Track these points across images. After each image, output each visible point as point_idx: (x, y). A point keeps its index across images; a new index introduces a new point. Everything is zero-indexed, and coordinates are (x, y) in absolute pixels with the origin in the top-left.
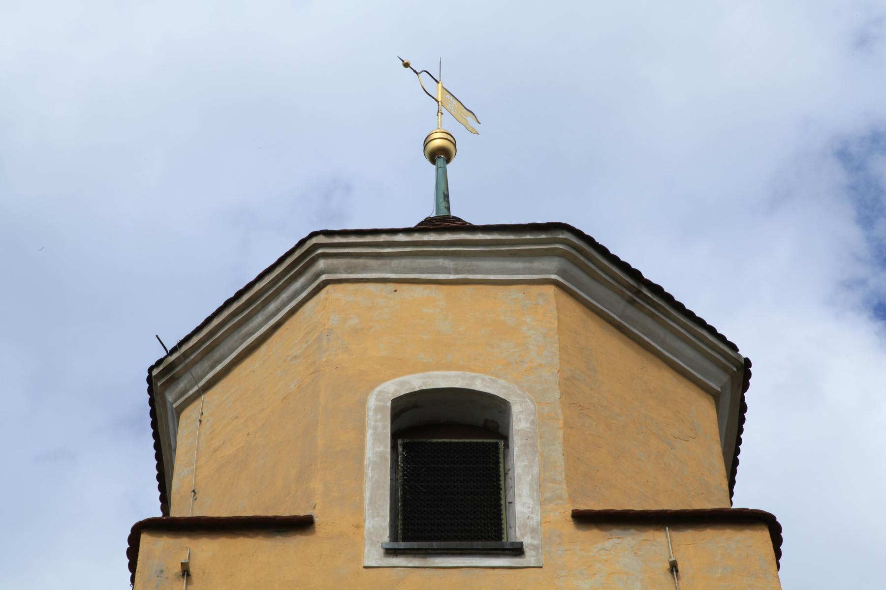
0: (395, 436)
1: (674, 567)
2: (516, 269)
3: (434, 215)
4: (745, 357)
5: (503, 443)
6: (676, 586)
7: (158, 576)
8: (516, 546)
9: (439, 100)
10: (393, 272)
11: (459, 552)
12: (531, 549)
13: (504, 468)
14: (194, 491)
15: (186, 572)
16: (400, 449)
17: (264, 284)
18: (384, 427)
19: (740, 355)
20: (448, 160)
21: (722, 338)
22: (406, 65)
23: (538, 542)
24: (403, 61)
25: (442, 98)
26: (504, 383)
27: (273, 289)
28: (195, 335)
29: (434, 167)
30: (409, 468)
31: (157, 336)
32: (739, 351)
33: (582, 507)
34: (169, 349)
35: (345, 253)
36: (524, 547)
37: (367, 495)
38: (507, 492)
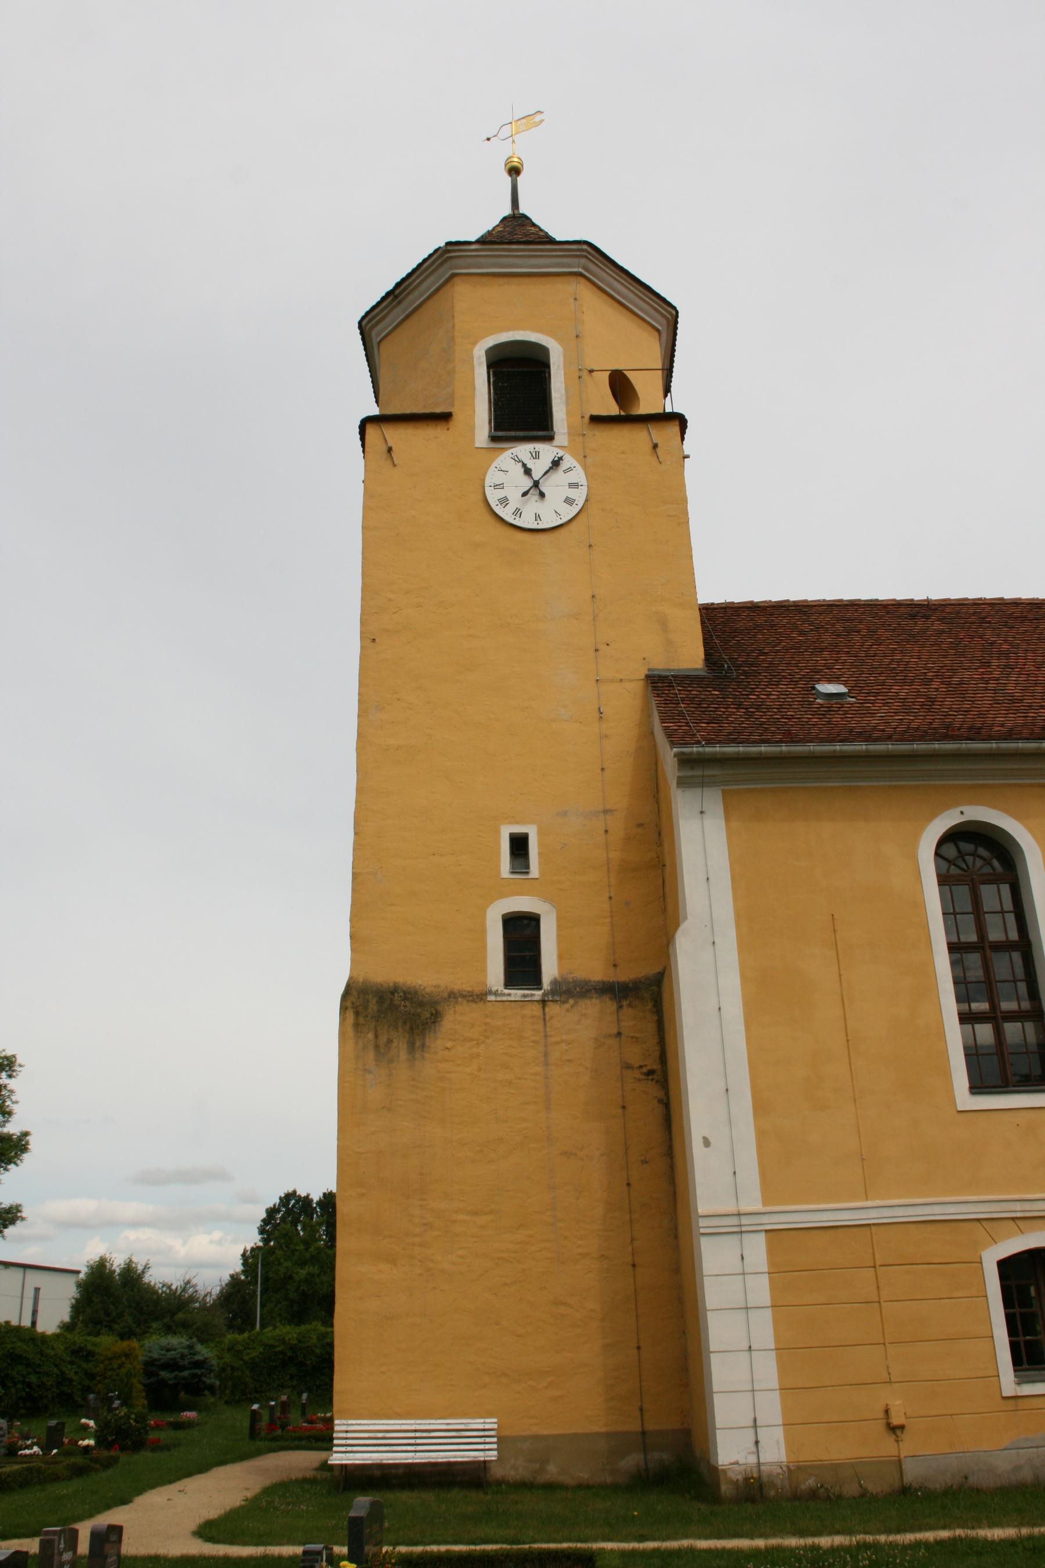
21: (430, 256)
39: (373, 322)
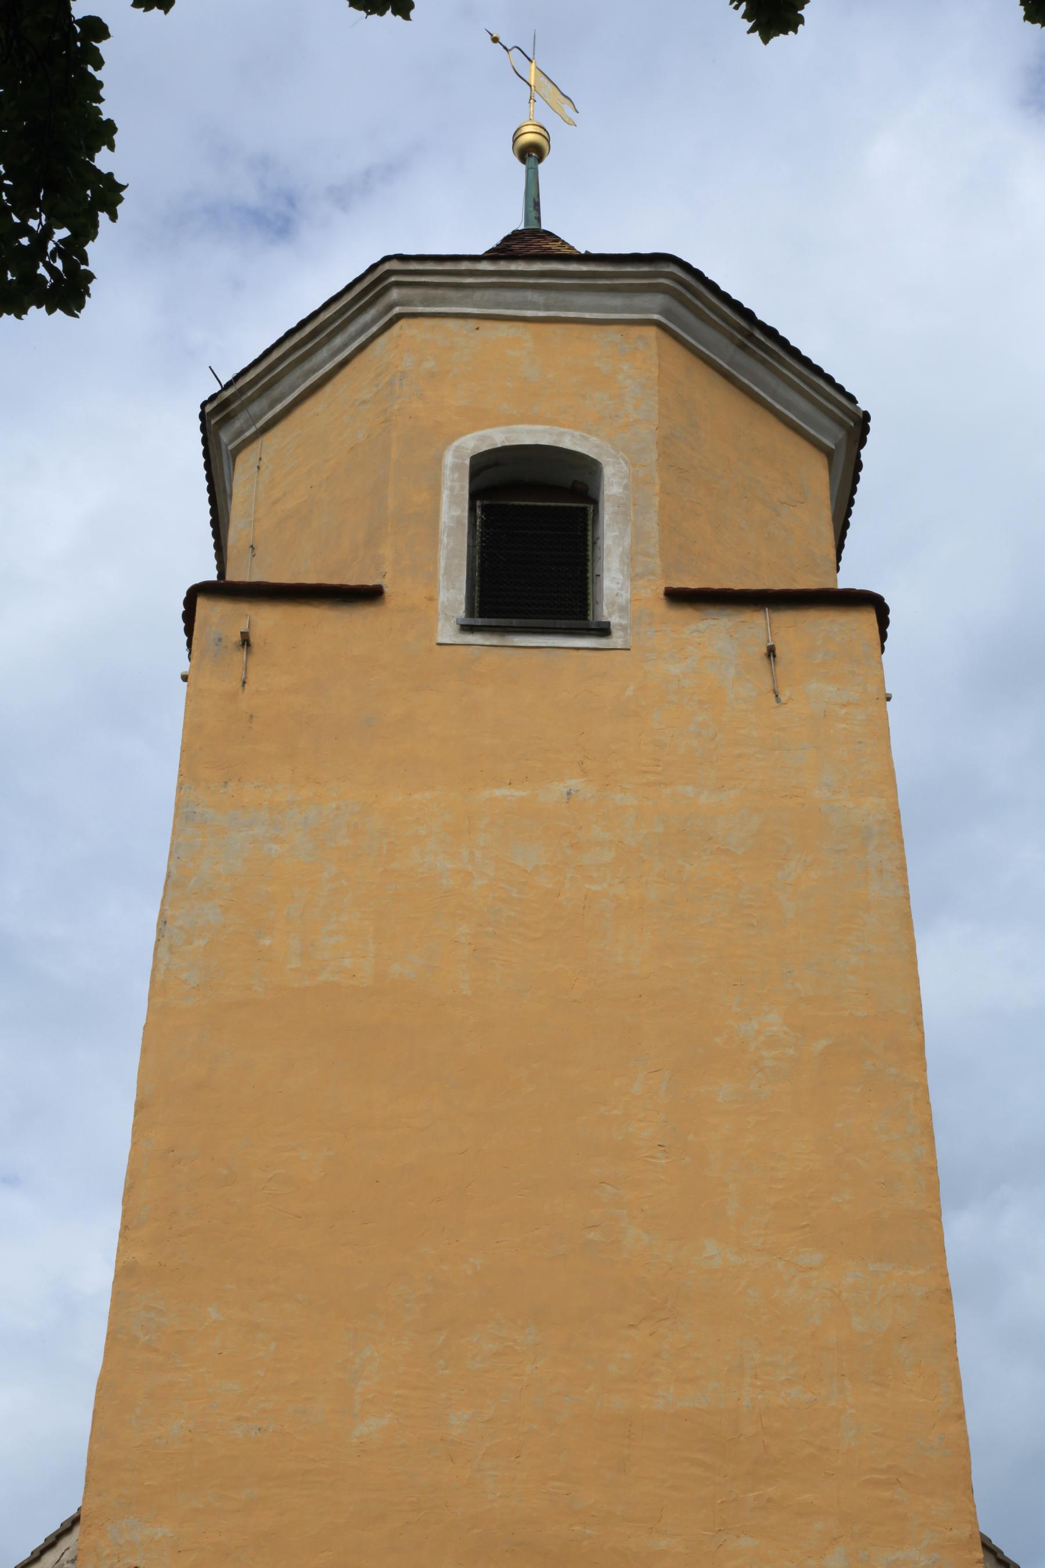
0: (473, 496)
1: (771, 652)
2: (613, 306)
3: (522, 227)
4: (864, 410)
5: (592, 509)
6: (772, 673)
7: (216, 645)
8: (602, 626)
9: (532, 83)
10: (475, 306)
11: (541, 630)
12: (618, 629)
13: (593, 536)
14: (252, 546)
15: (246, 641)
16: (479, 512)
17: (330, 315)
18: (462, 488)
19: (859, 408)
20: (540, 159)
21: (840, 389)
22: (495, 40)
23: (626, 622)
24: (491, 35)
25: (535, 81)
26: (594, 440)
27: (340, 321)
28: (253, 369)
29: (523, 167)
30: (488, 534)
31: (210, 367)
32: (857, 402)
33: (677, 584)
34: (223, 384)
35: (422, 282)
36: (611, 627)
37: (442, 563)
38: (595, 564)
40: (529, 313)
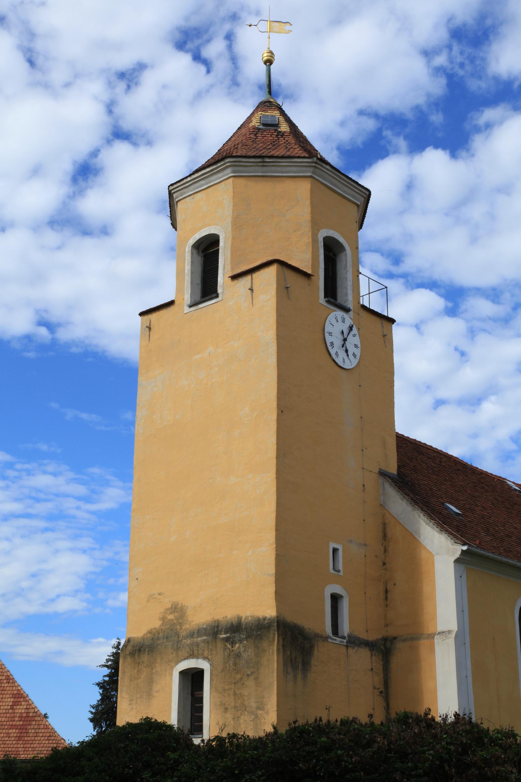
10: (192, 191)
39: (237, 164)
40: (203, 188)
